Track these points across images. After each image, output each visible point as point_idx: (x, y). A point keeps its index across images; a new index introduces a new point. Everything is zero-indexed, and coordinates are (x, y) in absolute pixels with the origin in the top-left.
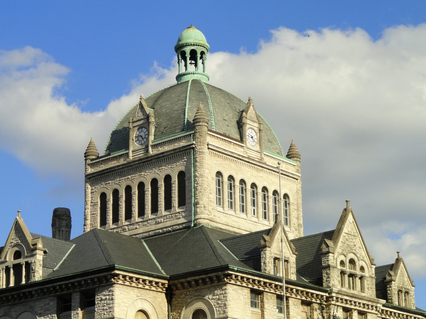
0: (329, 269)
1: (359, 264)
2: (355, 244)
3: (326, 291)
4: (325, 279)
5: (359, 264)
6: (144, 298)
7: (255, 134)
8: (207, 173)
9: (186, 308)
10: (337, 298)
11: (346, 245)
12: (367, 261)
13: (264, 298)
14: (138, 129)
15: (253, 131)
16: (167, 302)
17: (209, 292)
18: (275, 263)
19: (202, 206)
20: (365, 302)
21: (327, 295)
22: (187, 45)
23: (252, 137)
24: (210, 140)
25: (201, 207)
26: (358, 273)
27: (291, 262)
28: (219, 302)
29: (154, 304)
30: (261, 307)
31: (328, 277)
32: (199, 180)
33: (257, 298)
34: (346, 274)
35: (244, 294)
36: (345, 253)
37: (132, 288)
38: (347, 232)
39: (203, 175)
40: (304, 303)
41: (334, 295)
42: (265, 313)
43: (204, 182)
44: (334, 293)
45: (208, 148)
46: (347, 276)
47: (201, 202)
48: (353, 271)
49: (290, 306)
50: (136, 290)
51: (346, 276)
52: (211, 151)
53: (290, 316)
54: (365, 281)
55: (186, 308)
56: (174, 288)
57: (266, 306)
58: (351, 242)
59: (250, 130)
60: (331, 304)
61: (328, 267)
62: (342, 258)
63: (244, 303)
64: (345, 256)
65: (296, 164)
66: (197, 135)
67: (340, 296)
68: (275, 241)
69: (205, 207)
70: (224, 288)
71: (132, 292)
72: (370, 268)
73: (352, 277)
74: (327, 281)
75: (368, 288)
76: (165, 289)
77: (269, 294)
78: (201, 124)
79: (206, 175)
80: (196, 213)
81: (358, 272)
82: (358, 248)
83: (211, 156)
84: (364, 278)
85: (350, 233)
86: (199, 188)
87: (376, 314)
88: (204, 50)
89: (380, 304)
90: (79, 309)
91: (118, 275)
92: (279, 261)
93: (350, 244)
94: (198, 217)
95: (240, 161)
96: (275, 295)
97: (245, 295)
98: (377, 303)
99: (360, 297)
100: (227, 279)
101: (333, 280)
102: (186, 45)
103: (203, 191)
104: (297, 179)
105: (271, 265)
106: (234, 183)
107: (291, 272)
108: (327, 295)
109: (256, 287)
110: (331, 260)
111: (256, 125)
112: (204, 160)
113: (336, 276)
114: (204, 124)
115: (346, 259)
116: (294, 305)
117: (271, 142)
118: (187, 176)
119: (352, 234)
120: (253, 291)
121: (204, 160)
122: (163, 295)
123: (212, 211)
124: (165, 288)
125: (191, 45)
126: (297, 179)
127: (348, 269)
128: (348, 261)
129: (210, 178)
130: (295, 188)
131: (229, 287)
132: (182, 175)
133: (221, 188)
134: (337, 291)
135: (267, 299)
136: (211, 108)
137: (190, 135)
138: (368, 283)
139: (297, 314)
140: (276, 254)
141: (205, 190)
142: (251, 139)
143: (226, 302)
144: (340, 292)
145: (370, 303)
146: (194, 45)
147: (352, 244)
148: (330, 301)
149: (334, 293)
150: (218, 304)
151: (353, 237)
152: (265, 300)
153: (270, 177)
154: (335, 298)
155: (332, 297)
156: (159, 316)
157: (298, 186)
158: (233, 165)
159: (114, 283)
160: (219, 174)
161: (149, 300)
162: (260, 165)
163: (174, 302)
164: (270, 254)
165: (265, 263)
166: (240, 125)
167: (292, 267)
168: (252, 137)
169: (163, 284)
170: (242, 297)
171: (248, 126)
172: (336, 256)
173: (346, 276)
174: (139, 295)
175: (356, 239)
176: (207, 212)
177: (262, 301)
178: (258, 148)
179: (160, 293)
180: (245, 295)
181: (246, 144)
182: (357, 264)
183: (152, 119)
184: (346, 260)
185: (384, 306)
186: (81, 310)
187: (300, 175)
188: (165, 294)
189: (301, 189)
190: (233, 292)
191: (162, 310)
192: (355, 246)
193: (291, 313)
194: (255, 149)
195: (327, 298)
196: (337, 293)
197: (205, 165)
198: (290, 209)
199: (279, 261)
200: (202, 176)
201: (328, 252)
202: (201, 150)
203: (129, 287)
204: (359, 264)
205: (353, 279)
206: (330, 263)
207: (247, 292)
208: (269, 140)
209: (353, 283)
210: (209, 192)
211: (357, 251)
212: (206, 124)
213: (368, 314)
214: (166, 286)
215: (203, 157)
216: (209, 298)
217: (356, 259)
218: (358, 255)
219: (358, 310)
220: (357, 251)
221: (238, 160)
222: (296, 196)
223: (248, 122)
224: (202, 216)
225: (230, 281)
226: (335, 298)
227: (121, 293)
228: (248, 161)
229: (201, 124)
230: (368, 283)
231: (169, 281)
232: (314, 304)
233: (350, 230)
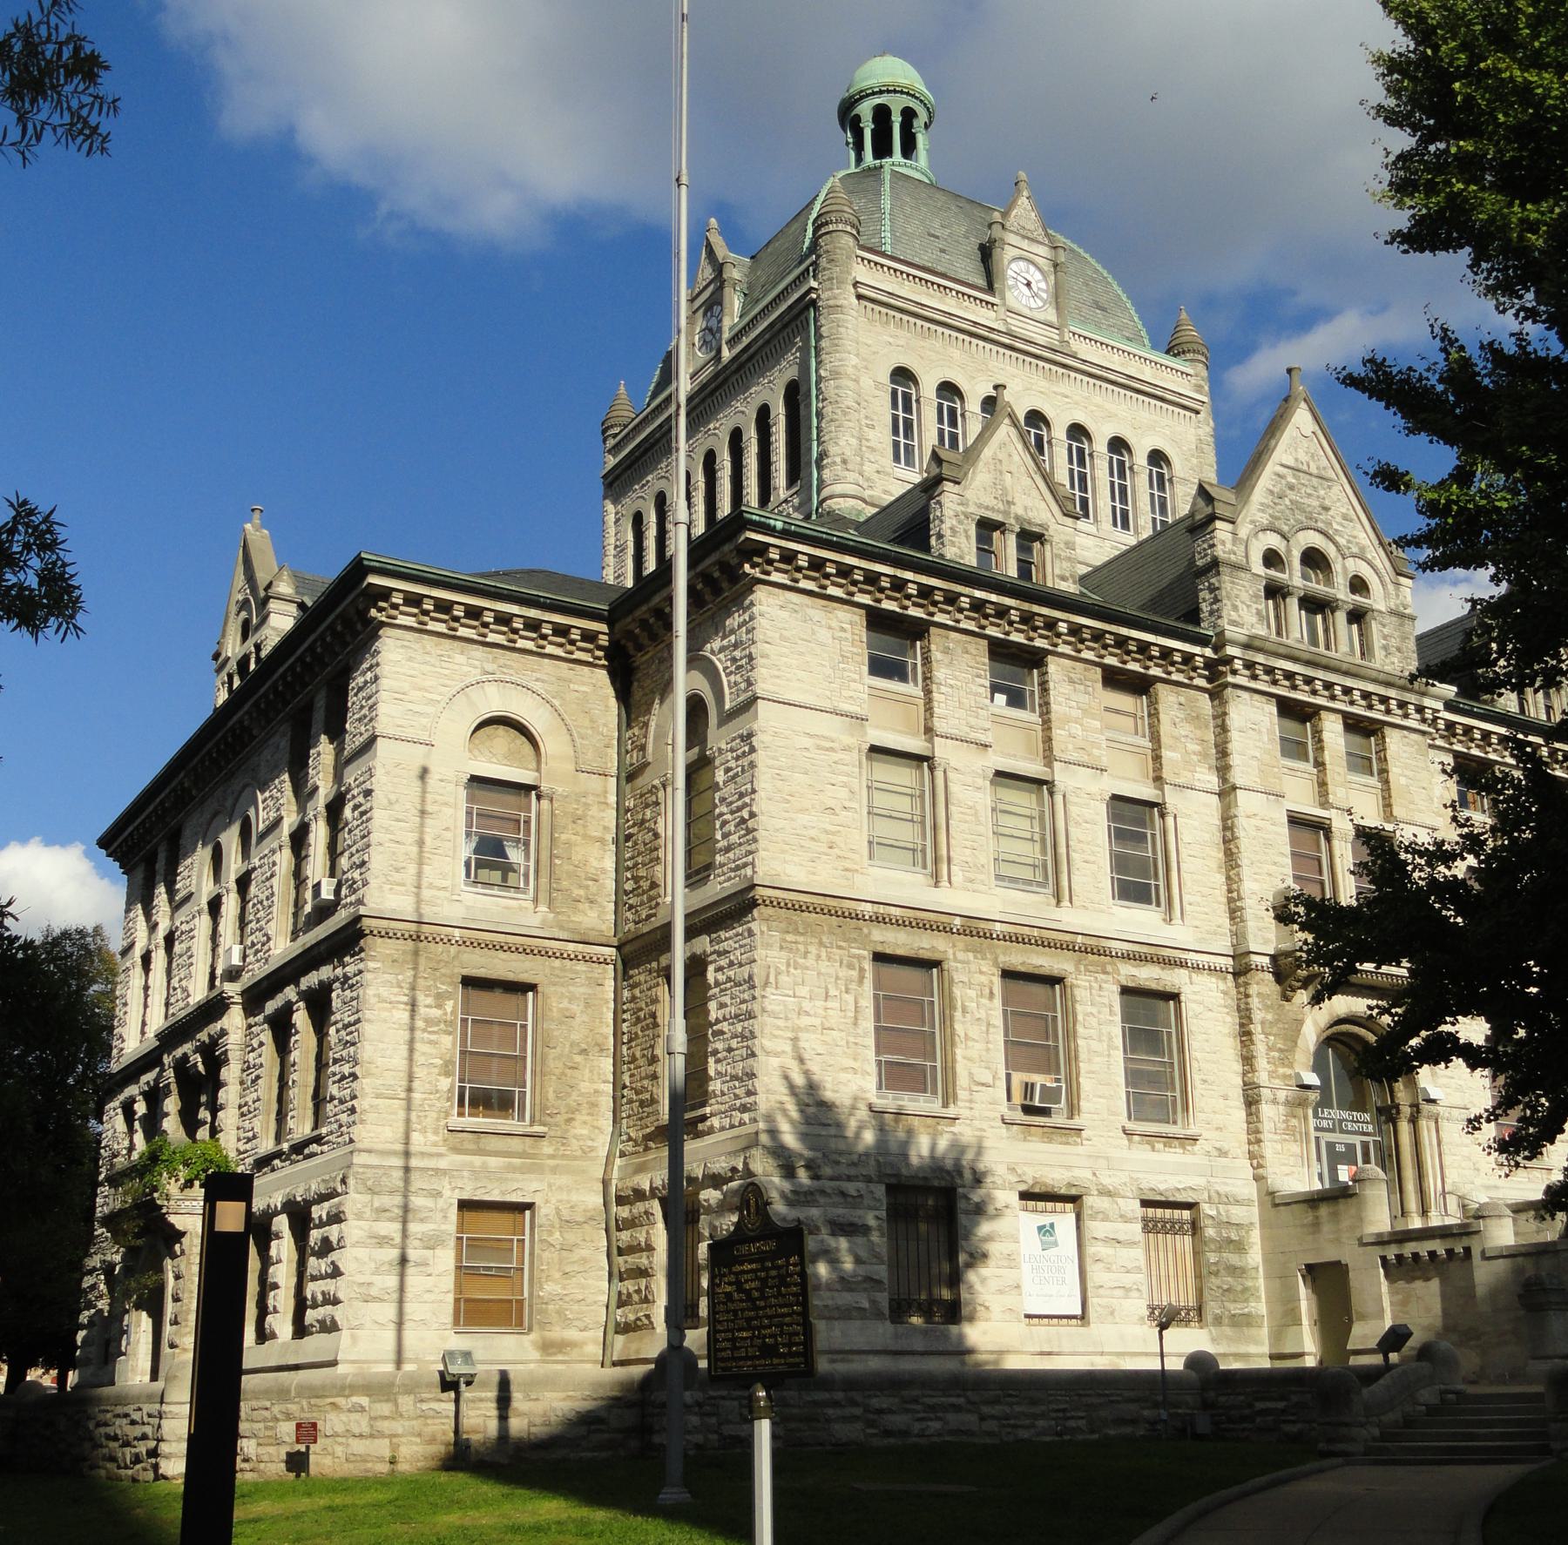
0: (1218, 573)
1: (1345, 568)
2: (1327, 503)
3: (1202, 641)
4: (1205, 607)
5: (1343, 569)
6: (514, 679)
7: (1038, 276)
8: (855, 367)
9: (662, 702)
10: (1250, 665)
11: (1287, 502)
12: (1380, 566)
13: (933, 647)
14: (705, 314)
15: (1032, 268)
16: (617, 698)
17: (712, 630)
18: (980, 539)
19: (838, 460)
20: (1371, 688)
21: (1208, 652)
22: (863, 96)
23: (1028, 285)
24: (861, 273)
25: (834, 463)
26: (1341, 596)
27: (1055, 539)
28: (737, 654)
29: (556, 702)
30: (925, 679)
31: (1216, 600)
32: (829, 388)
33: (911, 653)
34: (1290, 594)
35: (834, 624)
36: (1286, 528)
37: (456, 644)
38: (1291, 463)
39: (841, 370)
40: (1114, 679)
41: (1231, 650)
42: (935, 695)
43: (841, 392)
44: (1234, 643)
45: (860, 297)
46: (1296, 601)
47: (832, 449)
48: (1318, 587)
49: (1051, 685)
50: (478, 652)
51: (1293, 603)
52: (870, 305)
53: (1053, 716)
54: (1374, 626)
55: (662, 702)
56: (630, 646)
57: (940, 673)
58: (1309, 495)
59: (1022, 264)
60: (1226, 685)
61: (1215, 564)
62: (1273, 541)
63: (837, 658)
64: (1284, 537)
65: (1191, 371)
66: (823, 262)
67: (1260, 658)
68: (981, 464)
69: (844, 462)
70: (747, 602)
71: (461, 659)
72: (1391, 587)
73: (1323, 612)
74: (1211, 613)
75: (1385, 648)
76: (600, 654)
77: (953, 635)
78: (831, 227)
79: (850, 370)
80: (821, 484)
81: (1341, 592)
82: (1339, 519)
83: (871, 321)
84: (1368, 617)
85: (1305, 468)
86: (828, 410)
87: (1424, 733)
88: (913, 104)
89: (1436, 697)
90: (324, 738)
91: (386, 593)
92: (1003, 533)
93: (1305, 501)
94: (825, 493)
95: (981, 343)
96: (985, 642)
97: (843, 630)
98: (1424, 694)
99: (1345, 667)
100: (753, 567)
101: (1235, 608)
102: (862, 98)
103: (839, 416)
104: (1197, 412)
105: (963, 540)
106: (963, 408)
107: (1057, 571)
108: (1208, 652)
109: (888, 605)
110: (1223, 543)
111: (1043, 251)
112: (842, 330)
113: (1244, 596)
114: (841, 226)
115: (1288, 547)
116: (1071, 681)
117: (1104, 309)
118: (803, 389)
119: (1314, 470)
120: (877, 621)
121: (842, 330)
122: (603, 675)
123: (875, 476)
124: (600, 648)
125: (874, 93)
126: (1197, 412)
127: (1294, 576)
128: (1296, 555)
129: (866, 382)
130: (1193, 439)
131: (761, 595)
132: (795, 395)
133: (914, 417)
134: (1243, 639)
135: (946, 651)
136: (886, 203)
137: (807, 270)
138: (1386, 631)
139: (1084, 711)
140: (987, 508)
141: (845, 414)
142: (1025, 289)
143: (753, 649)
144: (1257, 643)
145: (1392, 693)
146: (881, 92)
147: (1316, 503)
148: (1223, 674)
149: (1234, 643)
150: (734, 660)
151: (1315, 481)
152: (936, 655)
153: (1098, 399)
154: (1238, 664)
155: (1229, 660)
156: (578, 741)
157: (1200, 432)
158: (956, 353)
159: (383, 624)
160: (902, 375)
161: (537, 686)
162: (1058, 360)
163: (637, 694)
164: (961, 504)
165: (940, 536)
166: (986, 253)
167: (1058, 556)
168: (1028, 285)
169: (589, 636)
170: (824, 635)
171: (1010, 252)
172: (1244, 530)
173: (1293, 603)
174: (490, 667)
175: (1330, 487)
176: (851, 476)
177: (927, 661)
178: (1052, 316)
179: (586, 669)
180: (843, 630)
181: (1003, 298)
182: (1337, 567)
183: (733, 274)
184: (1289, 551)
185: (1450, 706)
186: (331, 742)
187: (1205, 399)
188: (610, 673)
189: (1211, 440)
190: (784, 614)
191: (592, 721)
192: (1327, 509)
193: (1054, 707)
194: (1041, 317)
195: (1210, 664)
196: (1247, 646)
197: (848, 344)
198: (1173, 495)
199: (1003, 533)
200: (836, 374)
201: (1212, 518)
202: (831, 303)
203: (448, 641)
204: (1345, 568)
205: (1324, 620)
206: (1220, 551)
207: (850, 623)
208: (1096, 303)
209: (1326, 630)
210: (864, 421)
211: (1335, 526)
212: (849, 229)
213: (1388, 731)
214: (604, 640)
215: (839, 320)
216: (713, 652)
217: (1331, 551)
218: (1342, 541)
219: (1346, 716)
220: (1335, 526)
221: (975, 341)
222: (1195, 461)
223: (1012, 238)
224: (838, 489)
225: (768, 574)
226: (1238, 664)
227: (410, 659)
228: (1013, 346)
229: (831, 227)
230: (1386, 631)
231: (610, 625)
232: (1159, 686)
233: (1303, 457)
